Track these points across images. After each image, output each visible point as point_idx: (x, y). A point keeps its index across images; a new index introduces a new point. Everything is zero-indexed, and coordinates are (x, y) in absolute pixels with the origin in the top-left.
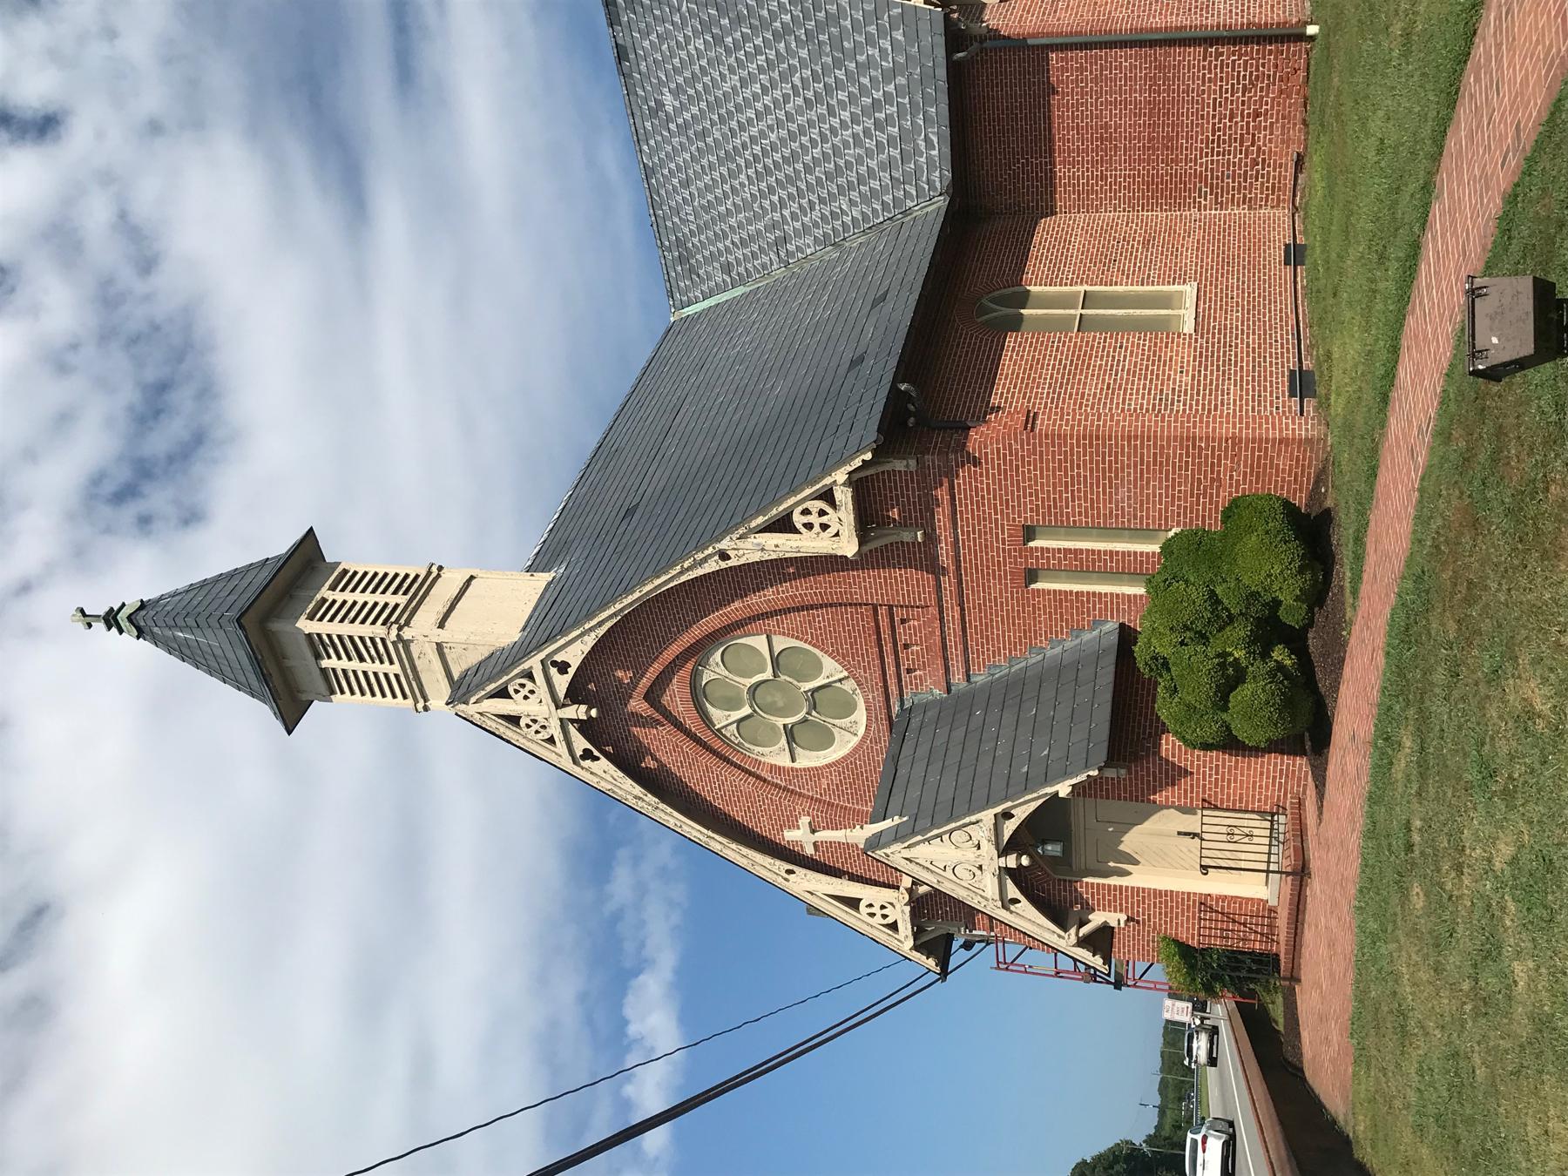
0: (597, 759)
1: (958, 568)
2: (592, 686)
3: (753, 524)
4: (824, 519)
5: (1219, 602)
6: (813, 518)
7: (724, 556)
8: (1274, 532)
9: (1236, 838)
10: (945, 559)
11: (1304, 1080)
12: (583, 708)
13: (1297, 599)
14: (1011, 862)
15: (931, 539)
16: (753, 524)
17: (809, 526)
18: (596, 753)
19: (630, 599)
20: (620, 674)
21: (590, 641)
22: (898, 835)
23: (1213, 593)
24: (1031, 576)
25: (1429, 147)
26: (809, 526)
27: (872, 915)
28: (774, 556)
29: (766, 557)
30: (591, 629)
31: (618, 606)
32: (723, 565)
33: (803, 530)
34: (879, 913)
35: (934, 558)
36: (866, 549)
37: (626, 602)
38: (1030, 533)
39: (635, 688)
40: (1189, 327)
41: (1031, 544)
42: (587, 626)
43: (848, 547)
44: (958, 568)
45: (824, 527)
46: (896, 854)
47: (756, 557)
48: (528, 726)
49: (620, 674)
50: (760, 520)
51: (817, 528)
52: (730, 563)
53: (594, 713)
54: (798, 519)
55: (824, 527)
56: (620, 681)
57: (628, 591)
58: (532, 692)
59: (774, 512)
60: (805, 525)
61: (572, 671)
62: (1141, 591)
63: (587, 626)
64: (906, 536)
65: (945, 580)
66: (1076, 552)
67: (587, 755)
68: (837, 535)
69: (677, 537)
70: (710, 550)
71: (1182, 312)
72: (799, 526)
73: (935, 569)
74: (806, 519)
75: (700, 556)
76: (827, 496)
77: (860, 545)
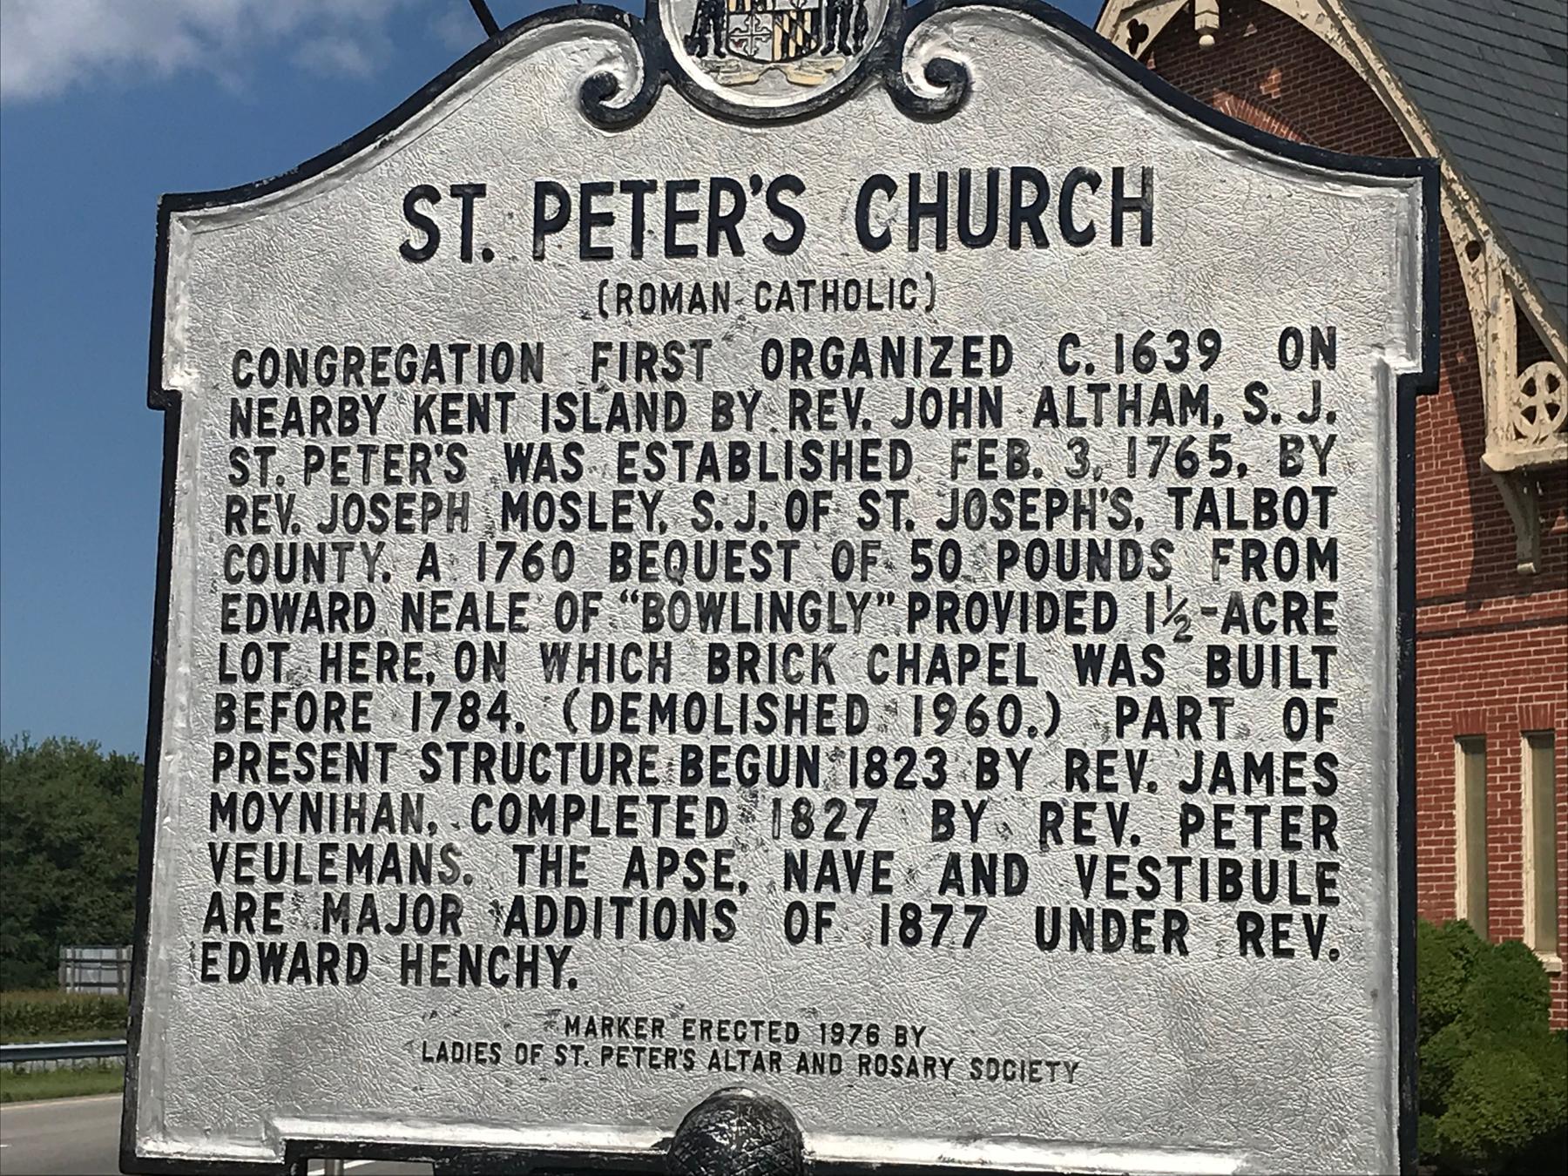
1: (1480, 629)
2: (1251, 30)
3: (1529, 298)
4: (1543, 414)
5: (1436, 1028)
6: (1543, 395)
7: (1475, 249)
8: (1544, 1105)
10: (1500, 607)
11: (827, 1164)
12: (1213, 21)
13: (1445, 1139)
15: (1523, 586)
16: (1529, 298)
17: (1530, 389)
19: (1396, 95)
20: (1275, 77)
21: (1324, 30)
23: (1449, 1019)
24: (1474, 746)
26: (1530, 389)
28: (1478, 333)
29: (1476, 321)
30: (1342, 30)
31: (1383, 75)
32: (1460, 249)
33: (1524, 380)
35: (1493, 593)
36: (1499, 482)
37: (1391, 88)
38: (1542, 740)
39: (1253, 103)
41: (1524, 743)
42: (1347, 23)
43: (1497, 457)
44: (1480, 629)
45: (1530, 414)
47: (1476, 304)
49: (1275, 77)
50: (1536, 309)
51: (1527, 402)
52: (1464, 260)
53: (1207, 40)
54: (1541, 370)
55: (1530, 414)
56: (1263, 78)
57: (1409, 91)
59: (1552, 332)
60: (1532, 381)
62: (1461, 913)
63: (1347, 23)
64: (1524, 545)
65: (1457, 610)
66: (1516, 815)
68: (1519, 435)
69: (1506, 162)
70: (1483, 227)
72: (1530, 372)
73: (1475, 594)
74: (1541, 383)
75: (1473, 211)
77: (1506, 474)
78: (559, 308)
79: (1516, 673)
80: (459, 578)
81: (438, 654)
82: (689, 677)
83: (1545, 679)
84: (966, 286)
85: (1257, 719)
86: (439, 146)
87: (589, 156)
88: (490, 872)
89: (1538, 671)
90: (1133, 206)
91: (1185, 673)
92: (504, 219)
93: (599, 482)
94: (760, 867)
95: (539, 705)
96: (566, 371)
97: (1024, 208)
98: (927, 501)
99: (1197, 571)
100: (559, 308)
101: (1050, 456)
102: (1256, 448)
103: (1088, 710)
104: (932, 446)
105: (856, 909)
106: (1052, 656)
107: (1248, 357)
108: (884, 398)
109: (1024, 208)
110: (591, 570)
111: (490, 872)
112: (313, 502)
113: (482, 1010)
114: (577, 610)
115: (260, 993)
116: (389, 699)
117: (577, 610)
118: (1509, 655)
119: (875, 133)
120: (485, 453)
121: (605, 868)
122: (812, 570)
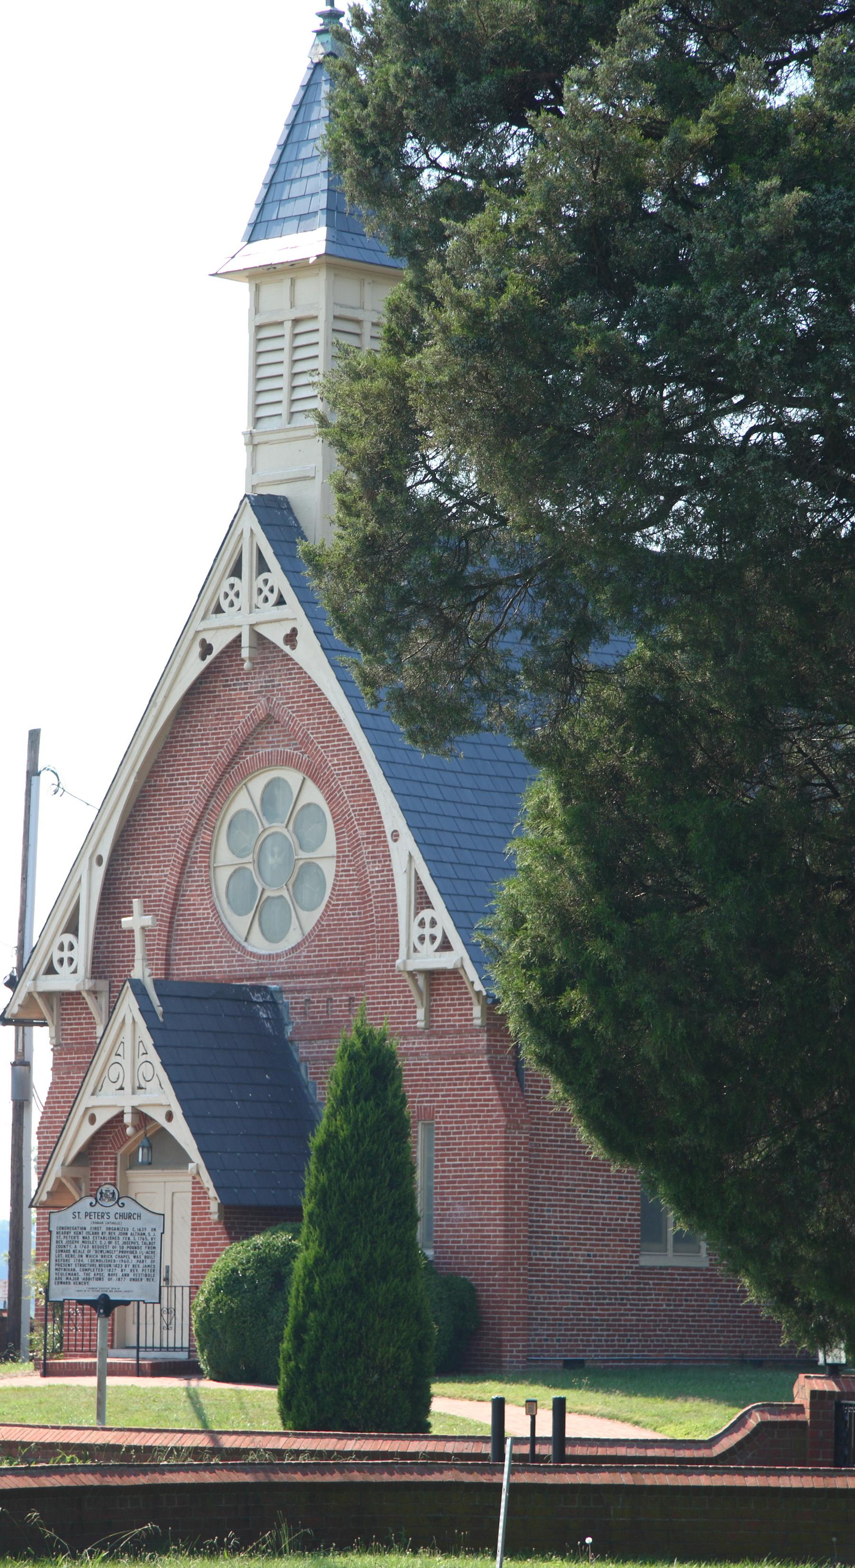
0: (203, 658)
9: (165, 1316)
14: (128, 1119)
18: (209, 658)
22: (146, 1011)
25: (148, 1358)
27: (61, 948)
34: (66, 954)
40: (646, 1261)
46: (129, 1005)
48: (232, 586)
54: (426, 914)
58: (266, 600)
61: (287, 649)
67: (207, 649)
71: (670, 1252)
76: (446, 946)
78: (88, 1223)
79: (416, 1086)
80: (78, 1249)
81: (77, 1255)
82: (99, 1258)
83: (430, 1091)
84: (125, 1223)
85: (148, 1262)
86: (76, 1208)
87: (90, 1209)
88: (82, 1275)
89: (427, 1085)
90: (139, 1216)
91: (143, 1258)
92: (82, 1215)
93: (91, 1239)
94: (106, 1273)
95: (86, 1261)
96: (88, 1229)
97: (130, 1216)
98: (121, 1242)
99: (144, 1250)
100: (88, 1223)
101: (132, 1238)
102: (149, 1238)
103: (134, 1261)
104: (121, 1237)
105: (114, 1278)
106: (131, 1256)
107: (149, 1230)
108: (117, 1232)
109: (130, 1216)
110: (91, 1248)
111: (82, 1275)
112: (64, 1241)
113: (80, 1287)
114: (89, 1251)
115: (61, 1286)
116: (72, 1261)
117: (89, 1251)
118: (412, 1075)
119: (116, 1209)
120: (81, 1237)
121: (92, 1275)
122: (111, 1248)
